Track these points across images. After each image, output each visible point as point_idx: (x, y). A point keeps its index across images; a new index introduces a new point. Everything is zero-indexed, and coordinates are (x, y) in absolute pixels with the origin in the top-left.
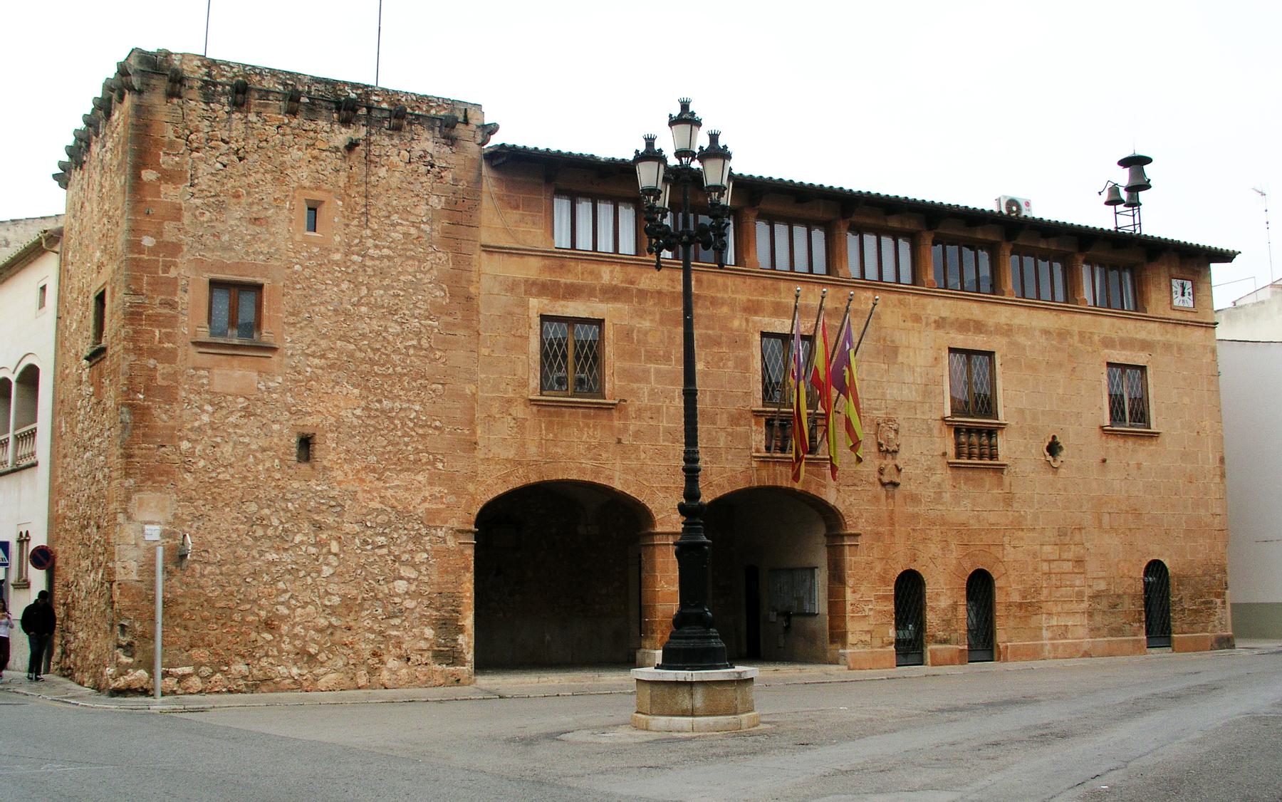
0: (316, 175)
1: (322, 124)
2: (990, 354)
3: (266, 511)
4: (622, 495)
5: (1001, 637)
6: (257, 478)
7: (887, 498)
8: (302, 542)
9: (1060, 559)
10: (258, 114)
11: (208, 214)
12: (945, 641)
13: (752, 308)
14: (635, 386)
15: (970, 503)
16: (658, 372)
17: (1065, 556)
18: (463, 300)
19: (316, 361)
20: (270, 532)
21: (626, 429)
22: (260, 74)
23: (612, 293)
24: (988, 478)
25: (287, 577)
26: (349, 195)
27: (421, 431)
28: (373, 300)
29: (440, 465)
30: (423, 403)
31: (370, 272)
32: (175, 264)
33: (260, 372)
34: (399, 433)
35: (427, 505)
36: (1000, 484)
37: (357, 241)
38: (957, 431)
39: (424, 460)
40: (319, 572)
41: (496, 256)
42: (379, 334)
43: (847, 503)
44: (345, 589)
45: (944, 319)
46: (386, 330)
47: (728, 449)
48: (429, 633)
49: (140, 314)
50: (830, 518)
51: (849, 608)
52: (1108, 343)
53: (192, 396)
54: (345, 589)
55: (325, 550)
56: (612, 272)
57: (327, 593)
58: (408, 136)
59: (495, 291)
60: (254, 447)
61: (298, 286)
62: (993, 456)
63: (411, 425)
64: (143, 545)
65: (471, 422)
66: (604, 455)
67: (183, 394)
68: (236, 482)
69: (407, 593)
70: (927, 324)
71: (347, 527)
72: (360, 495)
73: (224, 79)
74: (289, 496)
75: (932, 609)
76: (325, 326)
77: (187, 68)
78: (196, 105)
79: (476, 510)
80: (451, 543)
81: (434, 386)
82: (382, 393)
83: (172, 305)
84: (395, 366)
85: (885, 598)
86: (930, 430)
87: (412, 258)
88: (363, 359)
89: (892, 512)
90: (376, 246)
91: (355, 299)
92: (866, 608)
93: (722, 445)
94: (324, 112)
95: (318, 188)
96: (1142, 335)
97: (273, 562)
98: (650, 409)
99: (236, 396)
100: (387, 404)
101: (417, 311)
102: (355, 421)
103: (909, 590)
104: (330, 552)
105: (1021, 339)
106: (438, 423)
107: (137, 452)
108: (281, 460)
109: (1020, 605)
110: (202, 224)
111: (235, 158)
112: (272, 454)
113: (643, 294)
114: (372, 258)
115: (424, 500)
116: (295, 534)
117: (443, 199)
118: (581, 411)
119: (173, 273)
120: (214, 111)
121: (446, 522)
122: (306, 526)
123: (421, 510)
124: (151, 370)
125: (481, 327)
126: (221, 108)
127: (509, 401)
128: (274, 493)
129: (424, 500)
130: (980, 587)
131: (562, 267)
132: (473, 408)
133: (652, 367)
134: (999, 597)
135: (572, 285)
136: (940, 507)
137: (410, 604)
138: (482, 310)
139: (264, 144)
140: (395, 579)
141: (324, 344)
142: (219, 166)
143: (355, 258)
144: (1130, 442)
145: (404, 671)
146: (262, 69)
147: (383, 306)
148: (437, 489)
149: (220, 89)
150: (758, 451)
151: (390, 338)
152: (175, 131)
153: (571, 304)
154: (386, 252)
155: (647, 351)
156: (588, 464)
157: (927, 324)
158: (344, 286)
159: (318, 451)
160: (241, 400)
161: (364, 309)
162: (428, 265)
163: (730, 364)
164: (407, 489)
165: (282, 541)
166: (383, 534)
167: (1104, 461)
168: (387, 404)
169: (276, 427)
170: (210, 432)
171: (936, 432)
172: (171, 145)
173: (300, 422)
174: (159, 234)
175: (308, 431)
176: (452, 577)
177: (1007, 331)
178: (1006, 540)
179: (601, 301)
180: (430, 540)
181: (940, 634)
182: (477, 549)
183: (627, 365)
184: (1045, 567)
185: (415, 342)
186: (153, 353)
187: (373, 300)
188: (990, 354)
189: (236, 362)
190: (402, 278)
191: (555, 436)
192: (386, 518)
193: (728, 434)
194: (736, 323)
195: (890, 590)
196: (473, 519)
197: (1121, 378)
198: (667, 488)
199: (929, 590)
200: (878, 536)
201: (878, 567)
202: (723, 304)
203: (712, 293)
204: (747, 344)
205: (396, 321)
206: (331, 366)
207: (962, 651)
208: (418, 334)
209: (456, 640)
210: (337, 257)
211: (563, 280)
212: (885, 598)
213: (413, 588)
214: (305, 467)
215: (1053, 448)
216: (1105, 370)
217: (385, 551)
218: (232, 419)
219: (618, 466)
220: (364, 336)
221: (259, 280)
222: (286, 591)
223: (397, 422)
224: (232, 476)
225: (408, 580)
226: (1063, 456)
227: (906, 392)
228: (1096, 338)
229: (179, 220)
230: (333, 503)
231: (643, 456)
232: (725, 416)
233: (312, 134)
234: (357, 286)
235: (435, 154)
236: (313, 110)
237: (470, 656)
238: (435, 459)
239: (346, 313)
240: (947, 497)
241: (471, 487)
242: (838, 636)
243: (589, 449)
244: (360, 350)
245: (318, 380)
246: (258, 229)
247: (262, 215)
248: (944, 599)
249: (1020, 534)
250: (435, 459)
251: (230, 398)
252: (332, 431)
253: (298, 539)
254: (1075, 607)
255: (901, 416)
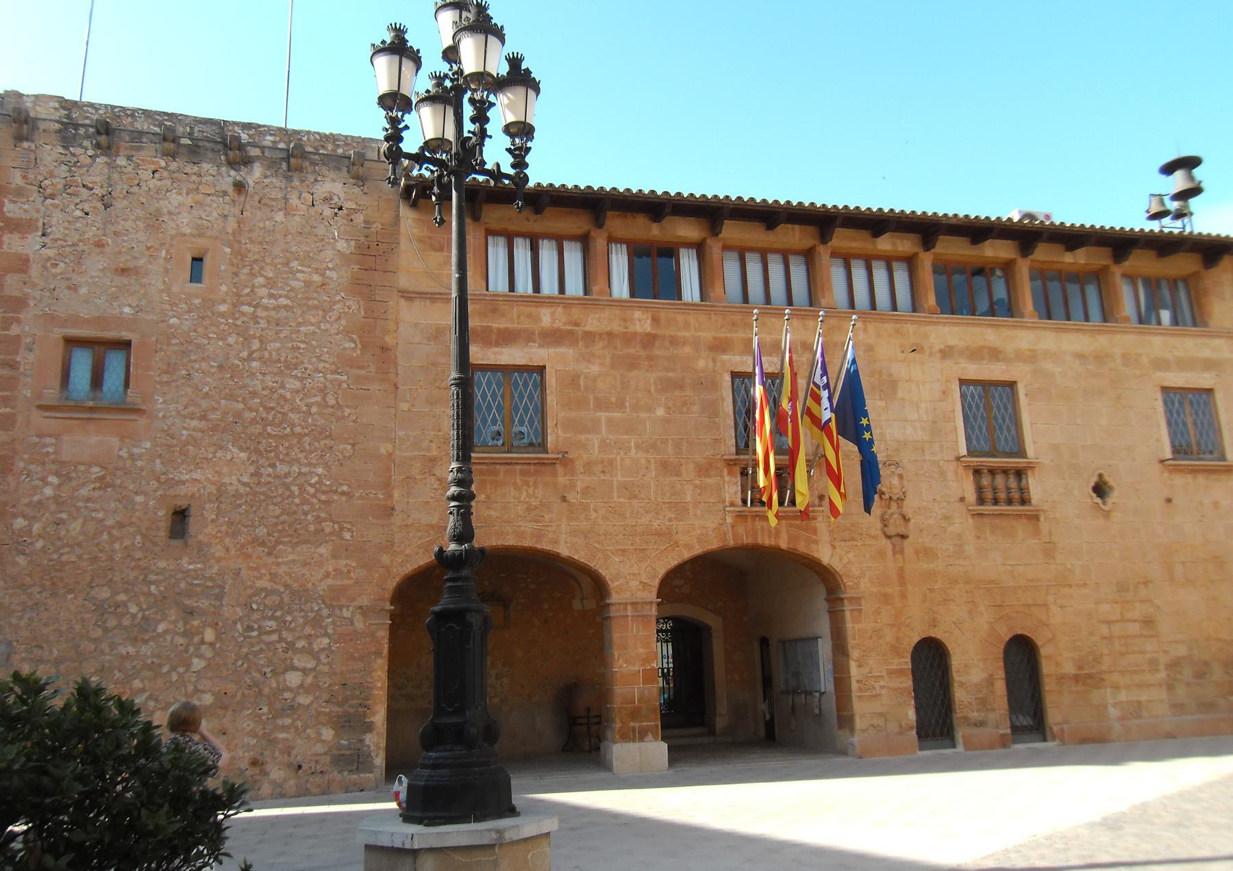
0: (200, 222)
1: (205, 166)
2: (1012, 385)
3: (122, 597)
4: (570, 562)
5: (1053, 716)
6: (111, 558)
7: (894, 552)
8: (166, 632)
9: (1123, 620)
10: (129, 158)
11: (62, 265)
12: (981, 724)
13: (719, 346)
14: (583, 437)
15: (1002, 556)
16: (610, 421)
17: (1129, 615)
18: (379, 353)
19: (194, 423)
20: (126, 622)
21: (573, 486)
22: (132, 115)
23: (554, 337)
24: (1021, 527)
25: (147, 673)
26: (240, 242)
27: (323, 497)
28: (267, 354)
30: (327, 466)
31: (263, 324)
32: (18, 321)
33: (122, 438)
34: (297, 501)
35: (330, 581)
36: (1036, 532)
37: (247, 291)
38: (977, 472)
39: (327, 530)
40: (188, 665)
41: (417, 303)
42: (273, 391)
43: (845, 561)
45: (951, 348)
46: (283, 386)
47: (696, 504)
48: (328, 734)
50: (827, 578)
51: (854, 686)
52: (1160, 364)
53: (32, 467)
55: (196, 639)
56: (552, 314)
57: (197, 690)
58: (312, 178)
59: (417, 340)
60: (109, 523)
61: (174, 341)
62: (1024, 501)
63: (312, 490)
65: (387, 486)
66: (547, 517)
67: (22, 464)
68: (84, 564)
69: (301, 686)
70: (931, 355)
71: (226, 611)
72: (244, 573)
73: (87, 122)
74: (153, 577)
75: (962, 684)
76: (207, 384)
77: (41, 112)
78: (50, 152)
79: (391, 585)
80: (359, 624)
81: (341, 447)
82: (277, 457)
83: (13, 365)
84: (293, 426)
85: (899, 672)
86: (942, 473)
87: (316, 307)
88: (254, 419)
89: (902, 569)
90: (271, 296)
91: (244, 354)
92: (877, 685)
93: (689, 499)
94: (210, 155)
95: (200, 235)
96: (1206, 353)
97: (128, 656)
98: (602, 461)
99: (90, 465)
100: (282, 468)
101: (321, 365)
102: (242, 490)
103: (931, 660)
104: (202, 642)
105: (1048, 366)
106: (345, 488)
108: (144, 536)
109: (1076, 678)
110: (55, 276)
111: (99, 205)
112: (132, 530)
113: (590, 337)
114: (266, 308)
115: (327, 575)
116: (158, 622)
117: (353, 243)
118: (518, 467)
119: (15, 330)
120: (74, 155)
121: (353, 600)
122: (173, 614)
123: (322, 587)
126: (84, 152)
127: (433, 460)
128: (132, 575)
129: (327, 575)
130: (1021, 655)
131: (494, 310)
132: (389, 470)
133: (603, 415)
134: (1047, 668)
135: (507, 330)
136: (961, 562)
137: (304, 700)
138: (401, 362)
139: (135, 189)
140: (286, 670)
141: (205, 404)
142: (79, 213)
143: (245, 309)
144: (1201, 478)
145: (292, 782)
146: (134, 111)
147: (279, 361)
148: (343, 562)
149: (82, 131)
150: (732, 505)
151: (288, 395)
152: (25, 177)
153: (506, 350)
154: (283, 301)
155: (596, 399)
156: (528, 527)
157: (931, 355)
158: (231, 340)
159: (193, 524)
160: (96, 469)
161: (254, 364)
162: (334, 315)
163: (695, 409)
164: (305, 564)
165: (141, 631)
166: (272, 618)
167: (1169, 500)
168: (282, 468)
169: (140, 499)
170: (53, 507)
171: (950, 475)
172: (20, 192)
173: (171, 492)
175: (183, 503)
176: (360, 665)
177: (1032, 357)
178: (1050, 599)
179: (541, 346)
180: (333, 623)
181: (975, 715)
182: (393, 630)
183: (573, 414)
184: (1104, 629)
185: (318, 399)
187: (267, 354)
188: (1012, 385)
190: (303, 329)
191: (488, 497)
192: (277, 599)
193: (696, 486)
194: (701, 364)
195: (906, 662)
196: (388, 595)
197: (1181, 404)
198: (624, 551)
199: (956, 662)
200: (886, 598)
201: (889, 636)
202: (684, 344)
203: (667, 332)
204: (714, 386)
205: (296, 377)
206: (215, 429)
207: (1002, 735)
208: (323, 391)
209: (362, 741)
210: (223, 308)
211: (495, 325)
212: (899, 672)
213: (309, 680)
214: (177, 543)
215: (1100, 489)
216: (1159, 395)
217: (275, 637)
218: (84, 492)
219: (563, 527)
220: (254, 394)
221: (125, 335)
222: (143, 690)
223: (295, 488)
224: (80, 557)
225: (305, 671)
226: (1113, 498)
227: (909, 431)
228: (1145, 360)
229: (25, 271)
230: (210, 584)
231: (594, 515)
232: (691, 466)
233: (194, 178)
234: (248, 339)
235: (342, 196)
236: (195, 152)
237: (379, 761)
238: (342, 529)
239: (234, 368)
240: (970, 549)
241: (386, 559)
242: (846, 721)
243: (529, 510)
244: (251, 410)
245: (196, 444)
246: (125, 280)
247: (131, 264)
248: (975, 673)
249: (1067, 590)
250: (342, 529)
251: (82, 468)
252: (210, 501)
253: (161, 628)
254: (1148, 677)
255: (906, 457)
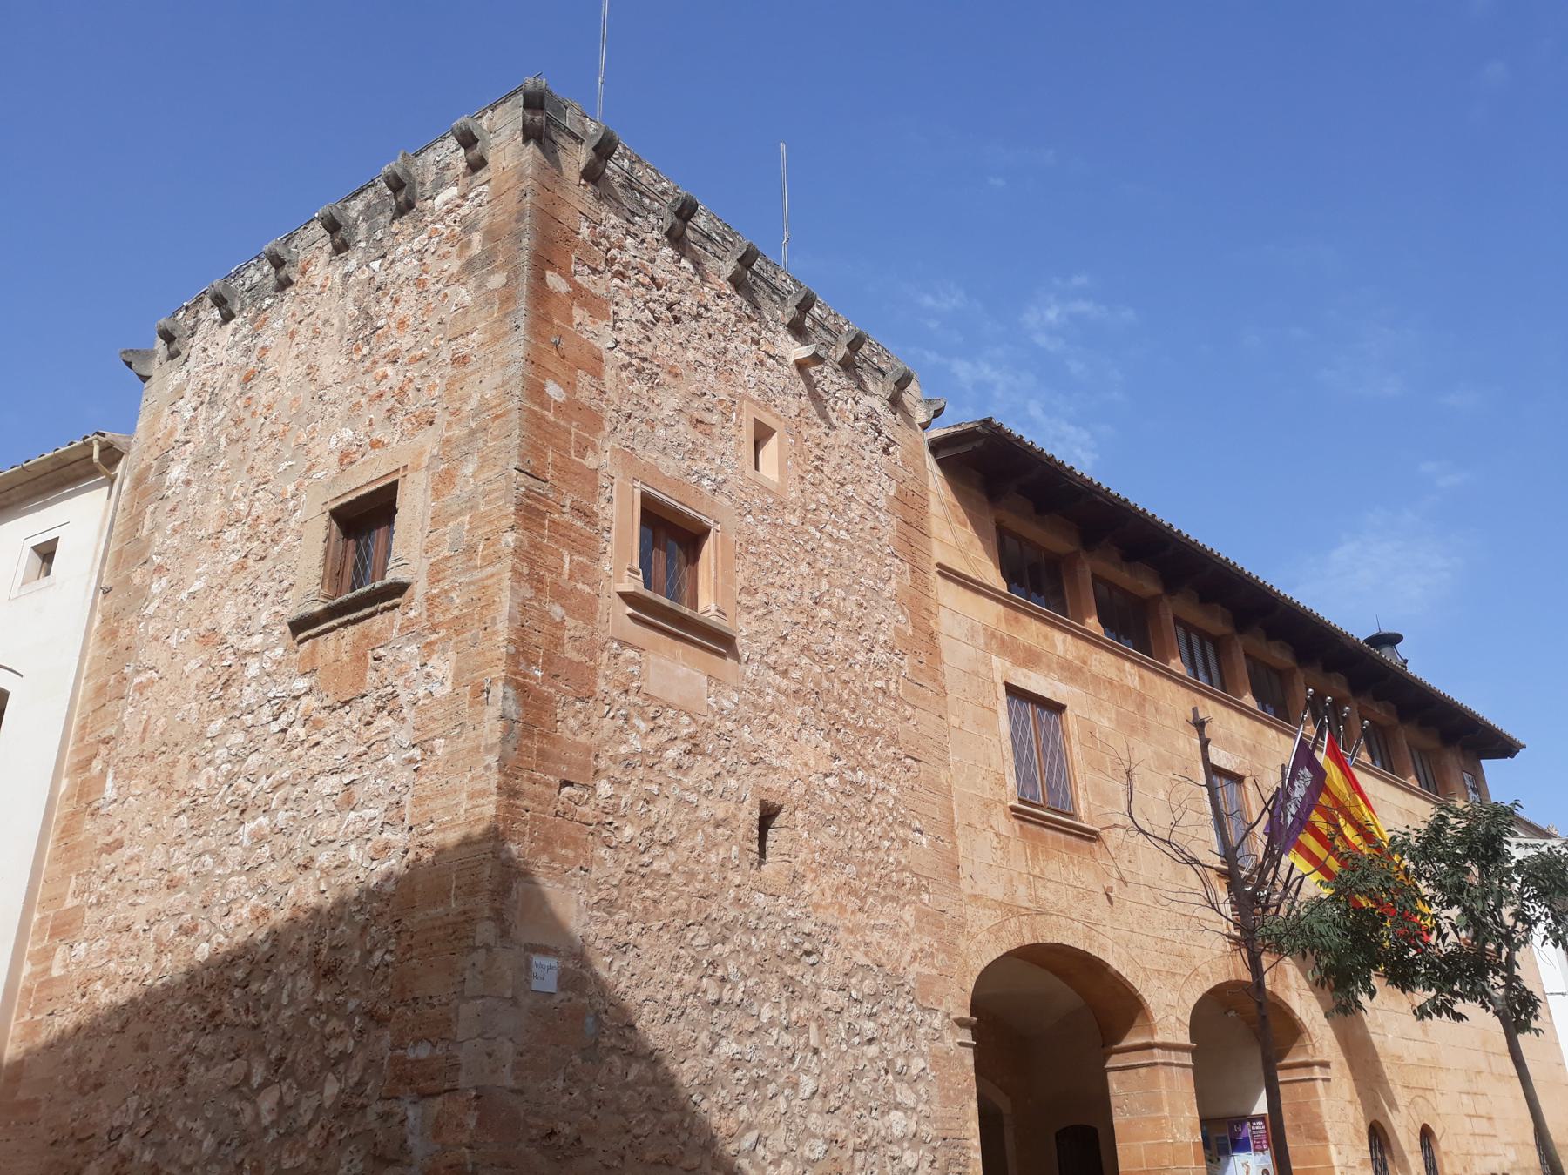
29: (925, 897)
44: (833, 1126)
49: (542, 514)
54: (833, 1126)
64: (526, 1001)
107: (526, 786)
119: (590, 461)
124: (555, 625)
125: (948, 682)
160: (686, 720)
174: (569, 386)
186: (560, 595)
189: (680, 647)
